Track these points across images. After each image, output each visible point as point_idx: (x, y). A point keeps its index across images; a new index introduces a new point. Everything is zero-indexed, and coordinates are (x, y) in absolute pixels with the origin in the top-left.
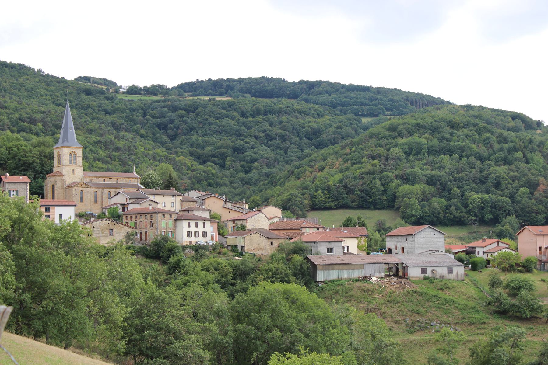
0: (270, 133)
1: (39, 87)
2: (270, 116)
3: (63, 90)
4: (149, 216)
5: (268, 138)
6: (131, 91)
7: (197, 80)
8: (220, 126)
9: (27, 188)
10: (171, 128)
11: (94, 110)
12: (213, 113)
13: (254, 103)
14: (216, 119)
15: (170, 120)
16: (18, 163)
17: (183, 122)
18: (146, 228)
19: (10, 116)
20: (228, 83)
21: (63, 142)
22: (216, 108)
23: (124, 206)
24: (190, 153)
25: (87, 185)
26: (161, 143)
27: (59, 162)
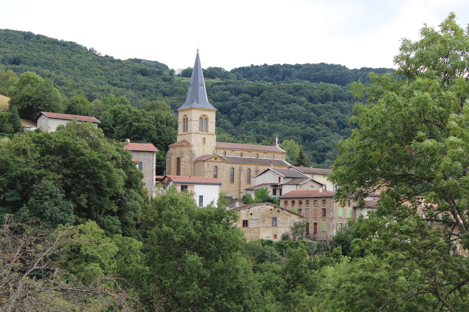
0: (342, 120)
1: (93, 66)
2: (340, 102)
3: (118, 70)
4: (320, 201)
5: (340, 125)
6: (187, 74)
7: (252, 66)
8: (288, 111)
9: (153, 160)
10: (234, 112)
11: (151, 91)
12: (279, 98)
13: (323, 88)
14: (282, 104)
15: (233, 104)
16: (129, 129)
17: (247, 106)
18: (315, 218)
19: (68, 93)
20: (285, 69)
21: (192, 102)
22: (281, 93)
23: (276, 187)
24: (256, 139)
25: (224, 160)
26: (224, 128)
27: (186, 129)
